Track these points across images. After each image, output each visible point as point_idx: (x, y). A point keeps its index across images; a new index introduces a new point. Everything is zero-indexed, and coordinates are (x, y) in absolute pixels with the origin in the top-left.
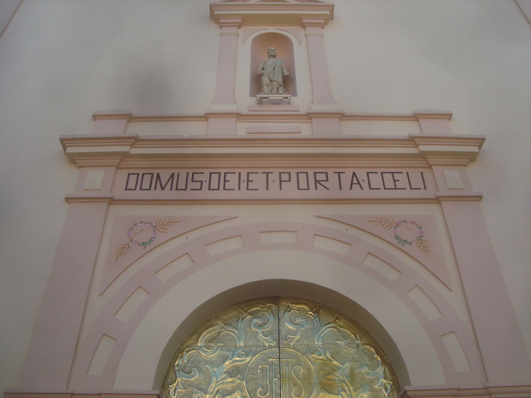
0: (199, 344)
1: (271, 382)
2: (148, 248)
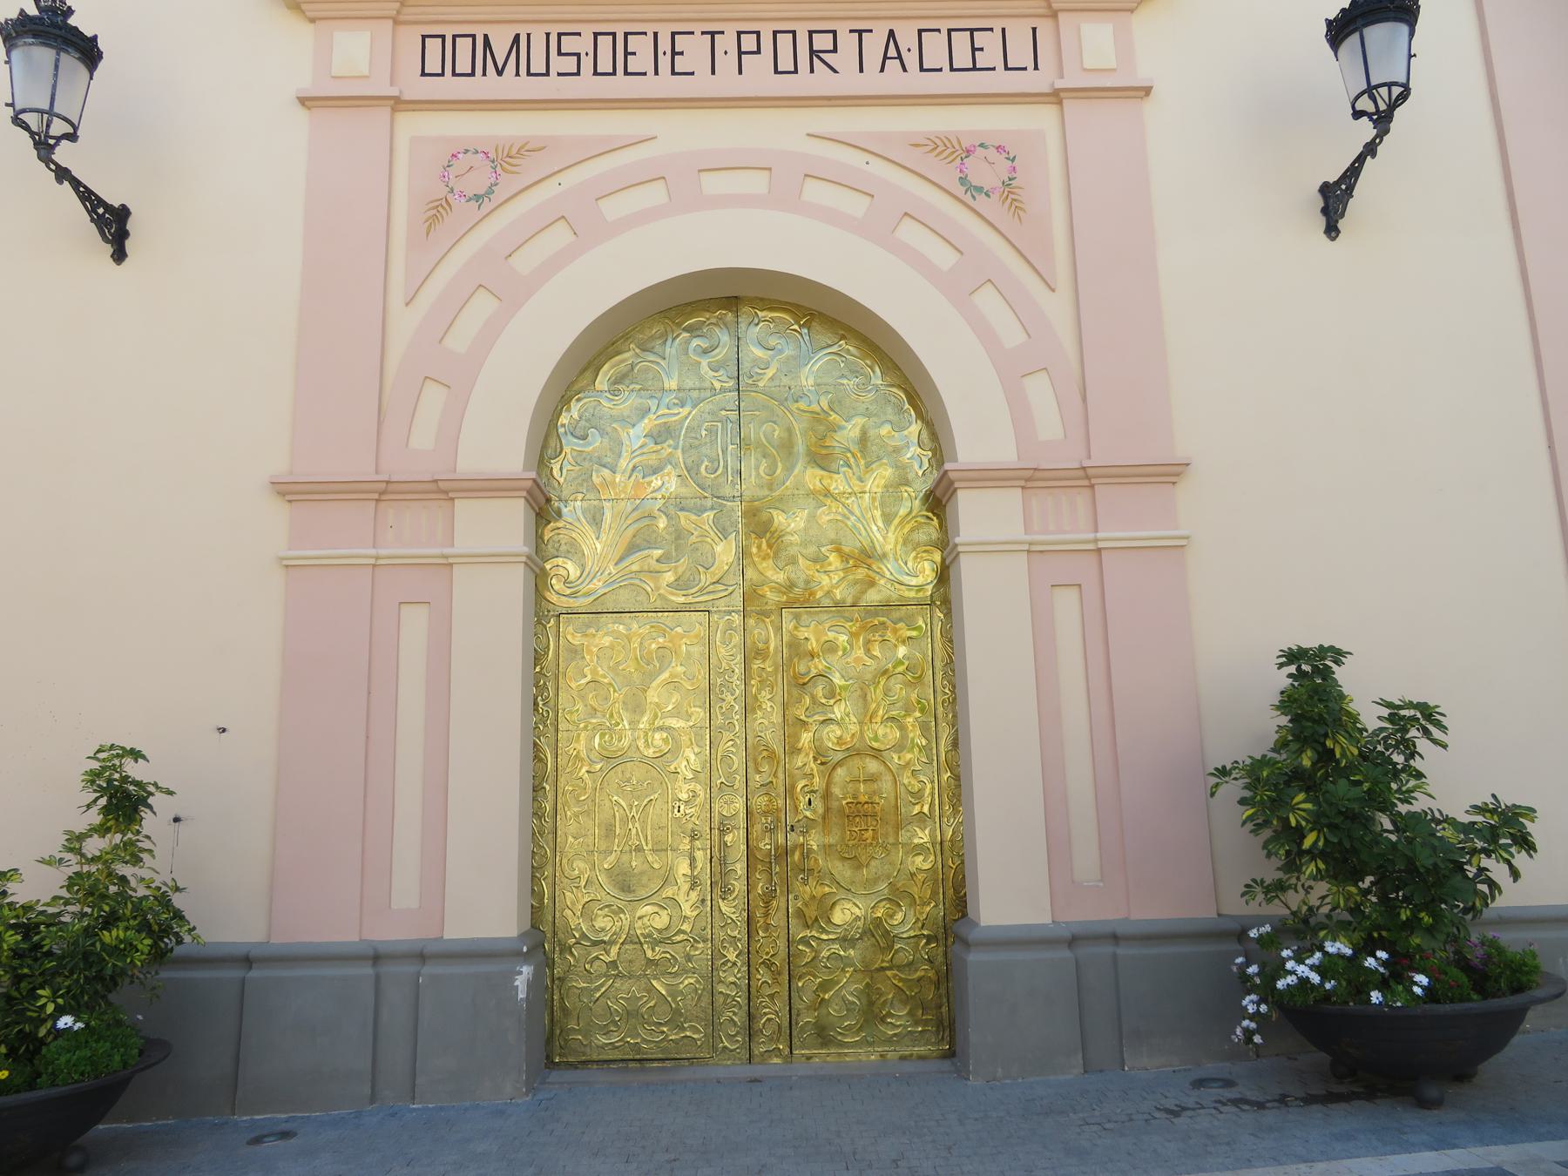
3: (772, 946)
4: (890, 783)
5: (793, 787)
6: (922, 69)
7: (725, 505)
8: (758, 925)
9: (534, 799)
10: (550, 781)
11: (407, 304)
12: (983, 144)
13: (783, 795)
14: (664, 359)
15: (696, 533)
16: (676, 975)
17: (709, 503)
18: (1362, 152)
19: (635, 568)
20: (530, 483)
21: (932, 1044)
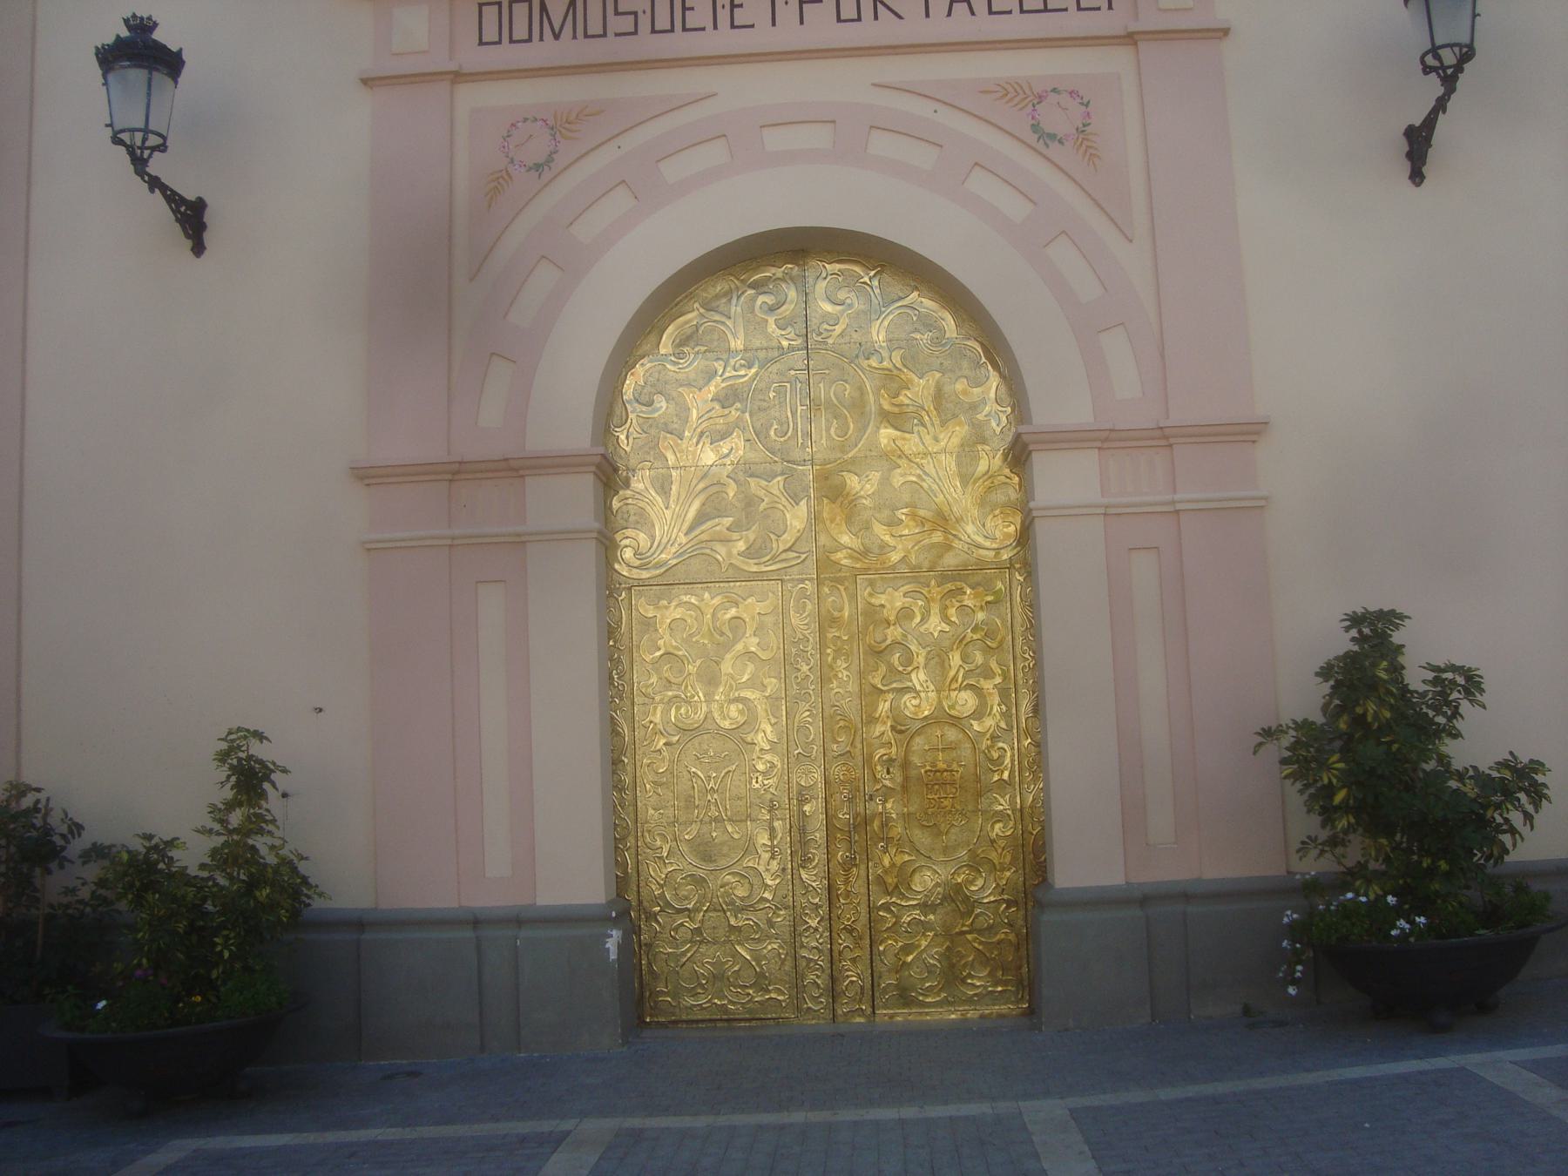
0: (663, 351)
1: (794, 414)
2: (547, 175)
3: (853, 914)
4: (969, 751)
5: (871, 756)
6: (991, 12)
7: (796, 470)
8: (839, 892)
9: (614, 772)
10: (628, 755)
11: (471, 280)
12: (1055, 89)
13: (861, 764)
14: (730, 318)
15: (766, 500)
16: (759, 940)
17: (778, 468)
18: (1435, 106)
19: (704, 537)
20: (598, 459)
21: (1012, 1003)
